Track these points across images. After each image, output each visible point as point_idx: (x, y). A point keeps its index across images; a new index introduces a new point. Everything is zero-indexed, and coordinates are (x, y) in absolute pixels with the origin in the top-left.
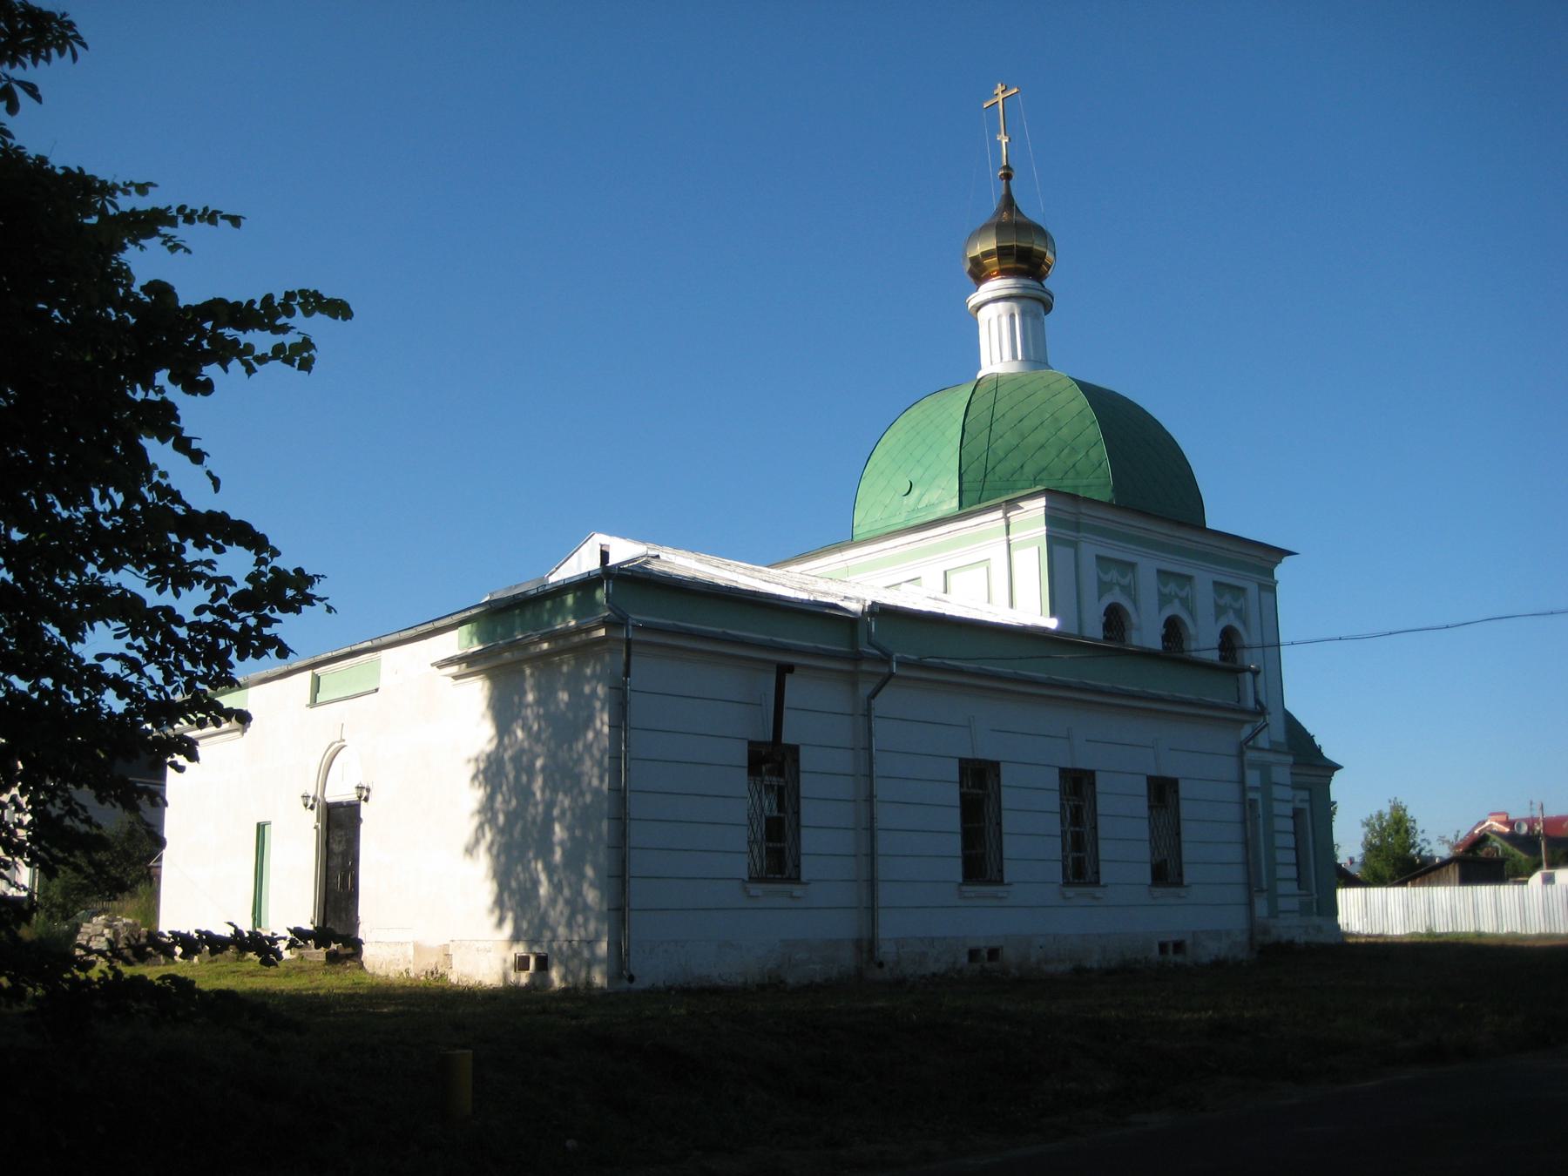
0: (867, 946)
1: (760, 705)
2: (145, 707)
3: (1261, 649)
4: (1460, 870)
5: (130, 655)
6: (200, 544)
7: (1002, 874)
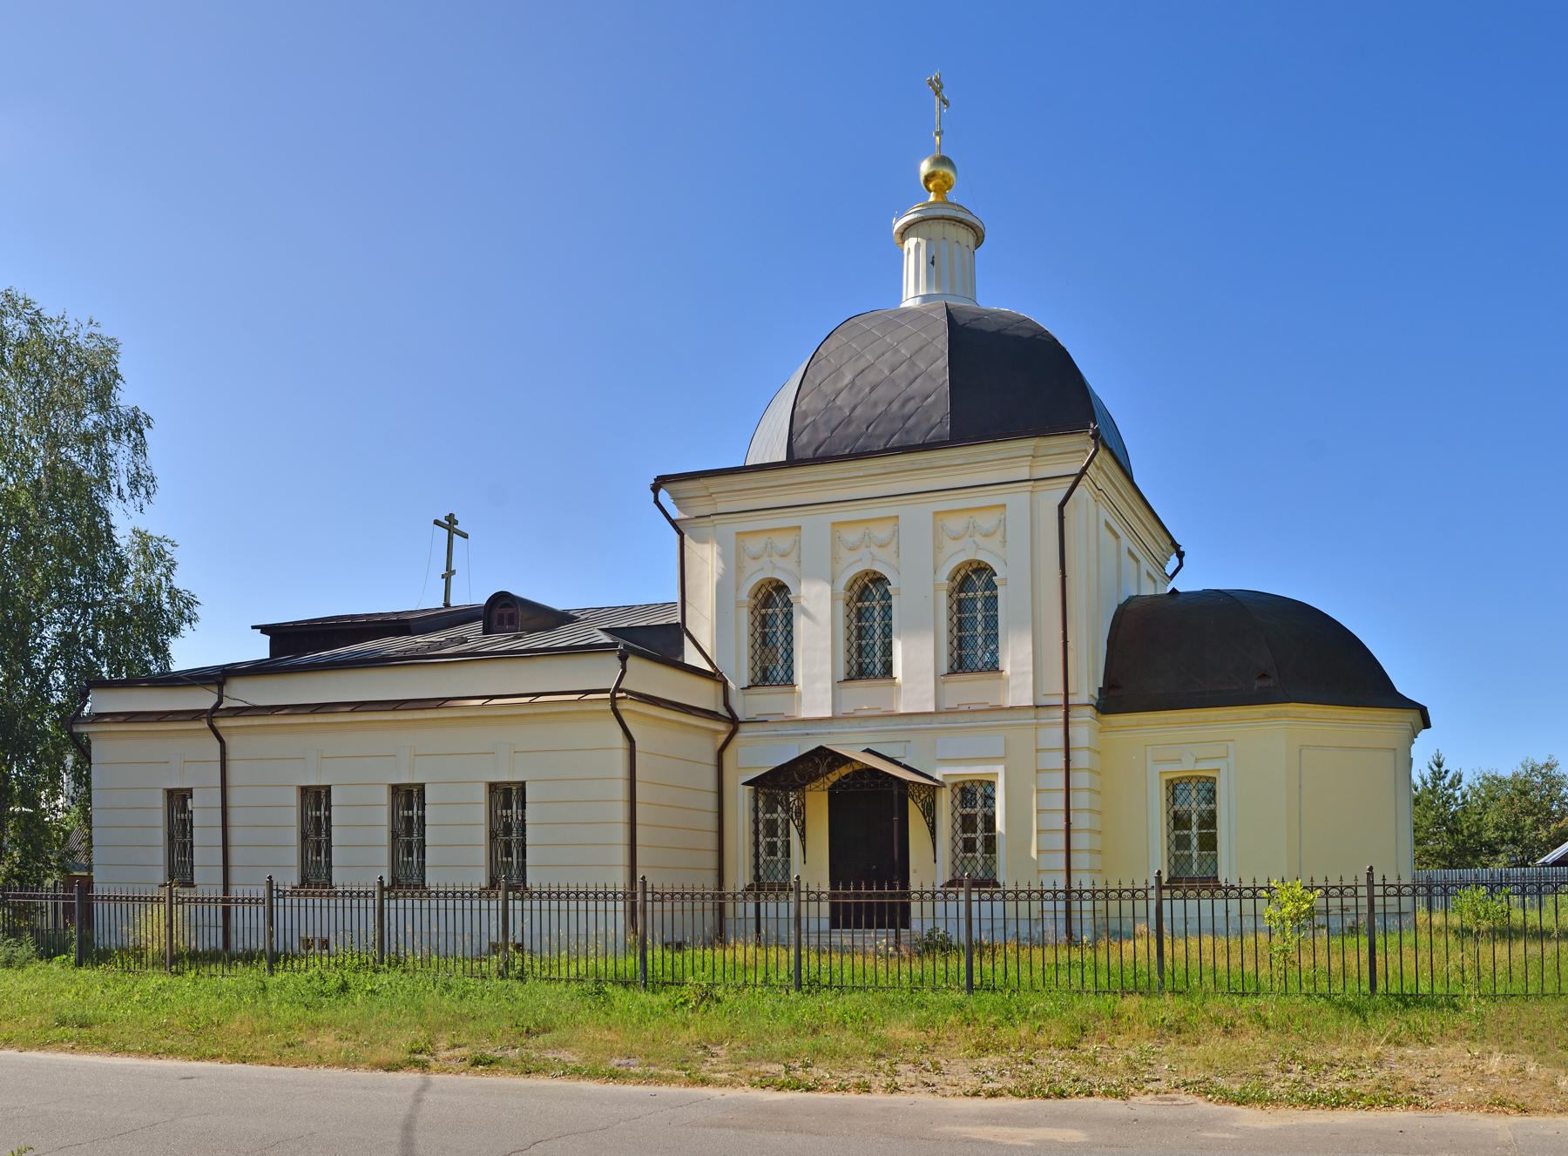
0: (623, 779)
1: (416, 755)
2: (92, 609)
3: (1402, 916)
4: (902, 647)
5: (85, 708)
6: (13, 789)
7: (934, 545)
